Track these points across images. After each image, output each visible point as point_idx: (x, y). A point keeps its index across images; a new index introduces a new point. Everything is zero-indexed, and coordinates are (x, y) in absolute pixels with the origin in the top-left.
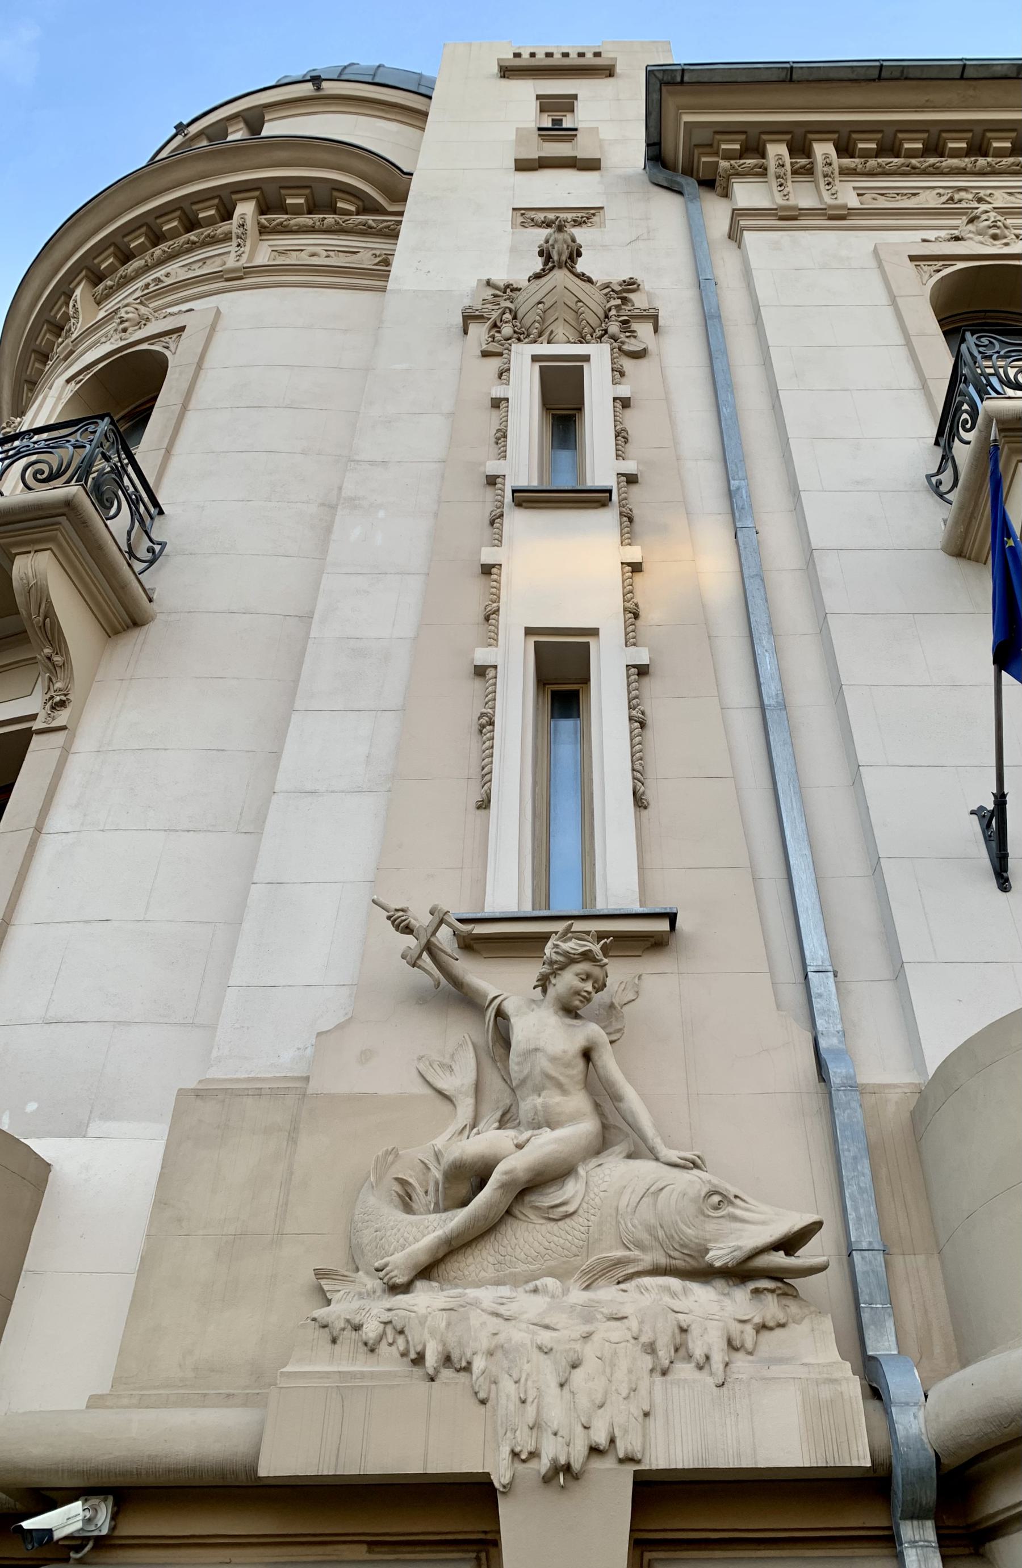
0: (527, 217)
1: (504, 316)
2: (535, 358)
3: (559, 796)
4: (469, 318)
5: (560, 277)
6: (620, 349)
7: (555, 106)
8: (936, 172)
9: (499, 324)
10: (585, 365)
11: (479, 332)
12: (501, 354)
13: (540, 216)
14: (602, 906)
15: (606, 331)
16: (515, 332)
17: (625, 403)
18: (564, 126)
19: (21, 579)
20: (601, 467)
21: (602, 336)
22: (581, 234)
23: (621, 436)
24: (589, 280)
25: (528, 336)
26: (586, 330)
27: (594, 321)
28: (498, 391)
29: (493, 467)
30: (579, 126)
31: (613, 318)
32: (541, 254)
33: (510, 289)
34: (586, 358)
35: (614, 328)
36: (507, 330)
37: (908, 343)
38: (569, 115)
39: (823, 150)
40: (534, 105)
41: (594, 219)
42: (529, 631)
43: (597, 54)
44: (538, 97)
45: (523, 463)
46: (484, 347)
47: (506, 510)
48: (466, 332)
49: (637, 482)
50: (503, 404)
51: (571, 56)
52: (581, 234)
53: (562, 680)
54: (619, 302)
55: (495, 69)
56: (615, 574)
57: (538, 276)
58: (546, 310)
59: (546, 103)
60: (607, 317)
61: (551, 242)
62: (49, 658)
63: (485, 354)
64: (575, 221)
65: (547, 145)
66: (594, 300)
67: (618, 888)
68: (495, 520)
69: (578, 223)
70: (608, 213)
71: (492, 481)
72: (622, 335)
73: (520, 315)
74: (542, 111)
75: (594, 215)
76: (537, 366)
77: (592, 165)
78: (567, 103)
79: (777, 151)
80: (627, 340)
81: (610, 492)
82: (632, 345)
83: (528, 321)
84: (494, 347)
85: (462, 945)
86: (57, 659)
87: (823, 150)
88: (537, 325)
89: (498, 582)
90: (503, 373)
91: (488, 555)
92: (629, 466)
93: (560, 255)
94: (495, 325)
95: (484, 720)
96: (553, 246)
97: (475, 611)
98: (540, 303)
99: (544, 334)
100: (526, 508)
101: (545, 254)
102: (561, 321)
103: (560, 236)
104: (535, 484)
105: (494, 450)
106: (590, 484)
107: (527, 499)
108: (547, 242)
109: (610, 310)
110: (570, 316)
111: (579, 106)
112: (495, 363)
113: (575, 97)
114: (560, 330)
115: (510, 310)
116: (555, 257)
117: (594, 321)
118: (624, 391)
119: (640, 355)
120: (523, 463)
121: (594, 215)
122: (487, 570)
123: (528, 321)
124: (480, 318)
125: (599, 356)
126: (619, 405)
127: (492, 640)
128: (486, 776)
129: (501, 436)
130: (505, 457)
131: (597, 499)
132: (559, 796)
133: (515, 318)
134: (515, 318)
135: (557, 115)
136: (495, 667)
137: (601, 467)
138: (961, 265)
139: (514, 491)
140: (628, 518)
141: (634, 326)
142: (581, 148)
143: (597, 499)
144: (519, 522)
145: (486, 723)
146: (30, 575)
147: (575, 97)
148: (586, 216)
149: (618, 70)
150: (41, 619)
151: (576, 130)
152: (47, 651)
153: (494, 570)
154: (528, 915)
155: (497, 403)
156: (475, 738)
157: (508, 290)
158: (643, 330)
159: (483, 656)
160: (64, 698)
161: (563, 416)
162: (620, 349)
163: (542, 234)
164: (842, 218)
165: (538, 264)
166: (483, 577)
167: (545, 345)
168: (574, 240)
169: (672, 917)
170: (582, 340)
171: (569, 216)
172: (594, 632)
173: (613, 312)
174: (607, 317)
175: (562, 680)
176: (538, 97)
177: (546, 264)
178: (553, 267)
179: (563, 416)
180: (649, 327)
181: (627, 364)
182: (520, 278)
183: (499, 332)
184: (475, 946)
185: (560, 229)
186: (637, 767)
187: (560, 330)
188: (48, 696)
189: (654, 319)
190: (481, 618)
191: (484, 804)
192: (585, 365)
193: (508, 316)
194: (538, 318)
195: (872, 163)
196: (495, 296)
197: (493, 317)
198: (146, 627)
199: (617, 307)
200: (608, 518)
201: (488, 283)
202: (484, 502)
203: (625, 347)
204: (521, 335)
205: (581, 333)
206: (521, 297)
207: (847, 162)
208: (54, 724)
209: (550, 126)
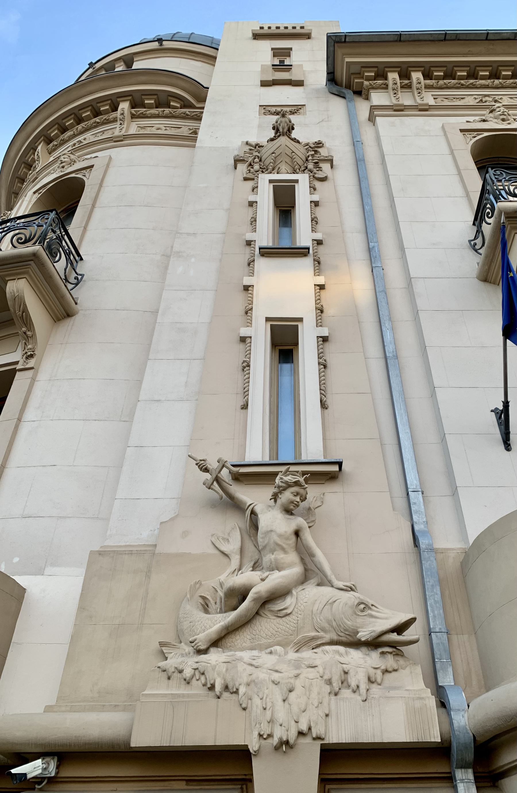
0: (266, 110)
1: (255, 160)
2: (271, 181)
3: (283, 403)
4: (237, 161)
5: (283, 140)
6: (314, 176)
7: (281, 54)
8: (473, 87)
9: (252, 164)
10: (296, 185)
11: (242, 168)
12: (253, 179)
13: (273, 109)
14: (304, 458)
15: (306, 168)
16: (260, 168)
17: (316, 204)
18: (285, 64)
19: (11, 293)
20: (304, 236)
21: (305, 170)
22: (294, 119)
23: (314, 220)
24: (298, 142)
25: (267, 170)
26: (296, 167)
27: (300, 162)
28: (252, 198)
29: (249, 236)
30: (293, 64)
31: (310, 161)
32: (274, 128)
33: (258, 146)
34: (297, 181)
35: (311, 166)
36: (256, 167)
37: (460, 174)
38: (288, 58)
39: (416, 76)
40: (270, 53)
41: (301, 111)
42: (268, 319)
43: (302, 28)
44: (272, 49)
45: (265, 234)
46: (245, 175)
47: (256, 258)
48: (236, 168)
49: (322, 244)
50: (255, 205)
51: (289, 28)
52: (294, 119)
53: (284, 344)
54: (313, 153)
55: (251, 35)
56: (311, 290)
57: (272, 140)
58: (276, 157)
59: (276, 52)
60: (307, 160)
61: (279, 122)
62: (25, 333)
63: (246, 179)
64: (291, 112)
65: (277, 73)
66: (300, 152)
67: (313, 449)
68: (250, 263)
69: (292, 113)
70: (308, 108)
71: (249, 243)
72: (315, 170)
73: (263, 160)
74: (274, 56)
75: (300, 108)
76: (272, 185)
77: (299, 83)
78: (287, 52)
79: (393, 76)
80: (317, 172)
81: (309, 249)
82: (320, 175)
83: (267, 163)
84: (250, 176)
85: (234, 478)
86: (29, 333)
87: (416, 76)
88: (272, 164)
89: (252, 294)
90: (254, 189)
91: (247, 281)
92: (318, 236)
93: (283, 129)
94: (250, 165)
95: (245, 364)
96: (280, 124)
97: (240, 309)
98: (273, 153)
99: (275, 169)
100: (266, 257)
101: (276, 128)
102: (284, 162)
103: (283, 120)
104: (270, 245)
105: (250, 228)
106: (298, 245)
107: (267, 252)
108: (277, 122)
109: (308, 157)
110: (288, 160)
111: (293, 53)
112: (250, 184)
113: (291, 49)
114: (284, 167)
115: (258, 157)
116: (281, 130)
117: (300, 162)
118: (315, 198)
119: (324, 179)
120: (265, 234)
121: (300, 108)
122: (246, 288)
123: (267, 163)
124: (243, 161)
125: (303, 180)
126: (313, 205)
127: (249, 324)
128: (246, 393)
129: (254, 221)
130: (256, 231)
131: (302, 252)
132: (283, 403)
133: (260, 161)
134: (260, 161)
135: (282, 58)
136: (251, 337)
137: (304, 236)
138: (486, 134)
139: (260, 249)
140: (318, 262)
141: (321, 165)
142: (294, 75)
143: (302, 252)
144: (262, 264)
145: (246, 366)
146: (15, 291)
147: (291, 49)
148: (297, 109)
149: (313, 35)
150: (21, 313)
151: (291, 66)
152: (24, 329)
153: (250, 288)
154: (267, 463)
155: (251, 204)
156: (240, 373)
157: (257, 147)
158: (325, 167)
159: (244, 332)
160: (32, 353)
161: (285, 210)
162: (314, 176)
163: (274, 118)
164: (426, 110)
165: (272, 134)
166: (244, 292)
167: (276, 174)
168: (290, 122)
169: (340, 464)
170: (294, 172)
171: (288, 109)
172: (301, 320)
173: (310, 158)
174: (307, 160)
175: (284, 344)
176: (272, 49)
177: (276, 133)
178: (280, 135)
179: (285, 210)
180: (329, 165)
181: (317, 184)
182: (263, 141)
183: (253, 168)
184: (240, 478)
185: (283, 116)
186: (322, 388)
187: (284, 167)
188: (24, 352)
189: (331, 161)
190: (244, 312)
191: (245, 407)
192: (296, 185)
193: (257, 160)
194: (272, 161)
195: (441, 82)
196: (251, 150)
197: (250, 161)
198: (74, 317)
199: (312, 155)
200: (308, 262)
201: (247, 143)
202: (245, 254)
203: (316, 176)
204: (263, 170)
205: (294, 168)
206: (263, 150)
207: (428, 82)
208: (27, 366)
209: (278, 63)
